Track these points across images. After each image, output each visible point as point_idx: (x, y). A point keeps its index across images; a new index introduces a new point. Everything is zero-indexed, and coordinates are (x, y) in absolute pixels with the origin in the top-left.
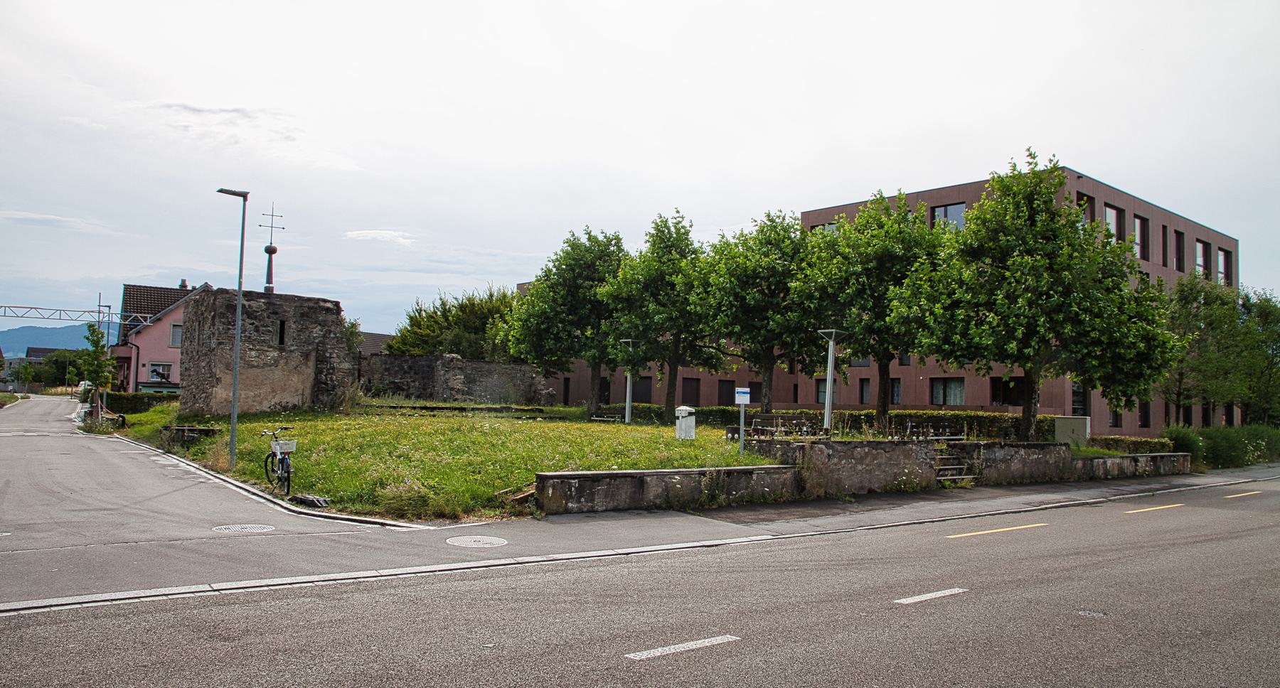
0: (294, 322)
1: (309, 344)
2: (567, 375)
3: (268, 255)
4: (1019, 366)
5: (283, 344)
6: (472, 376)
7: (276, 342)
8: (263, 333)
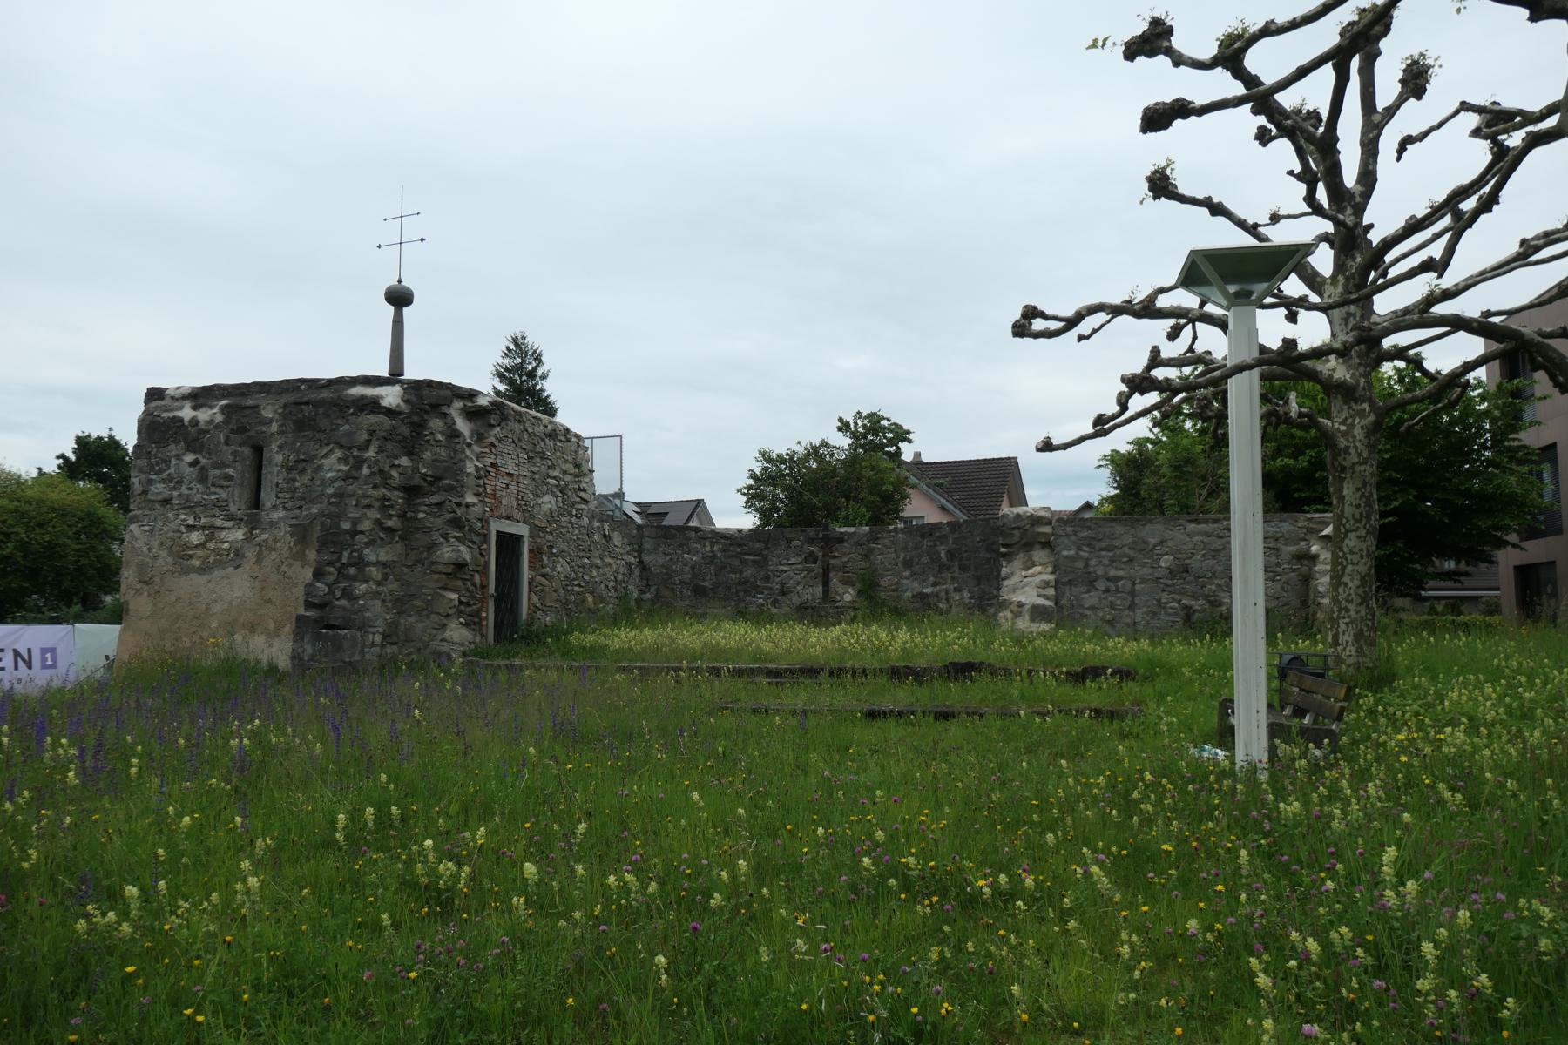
1: (312, 501)
2: (1536, 551)
4: (1476, 133)
5: (258, 509)
6: (1080, 564)
8: (214, 485)
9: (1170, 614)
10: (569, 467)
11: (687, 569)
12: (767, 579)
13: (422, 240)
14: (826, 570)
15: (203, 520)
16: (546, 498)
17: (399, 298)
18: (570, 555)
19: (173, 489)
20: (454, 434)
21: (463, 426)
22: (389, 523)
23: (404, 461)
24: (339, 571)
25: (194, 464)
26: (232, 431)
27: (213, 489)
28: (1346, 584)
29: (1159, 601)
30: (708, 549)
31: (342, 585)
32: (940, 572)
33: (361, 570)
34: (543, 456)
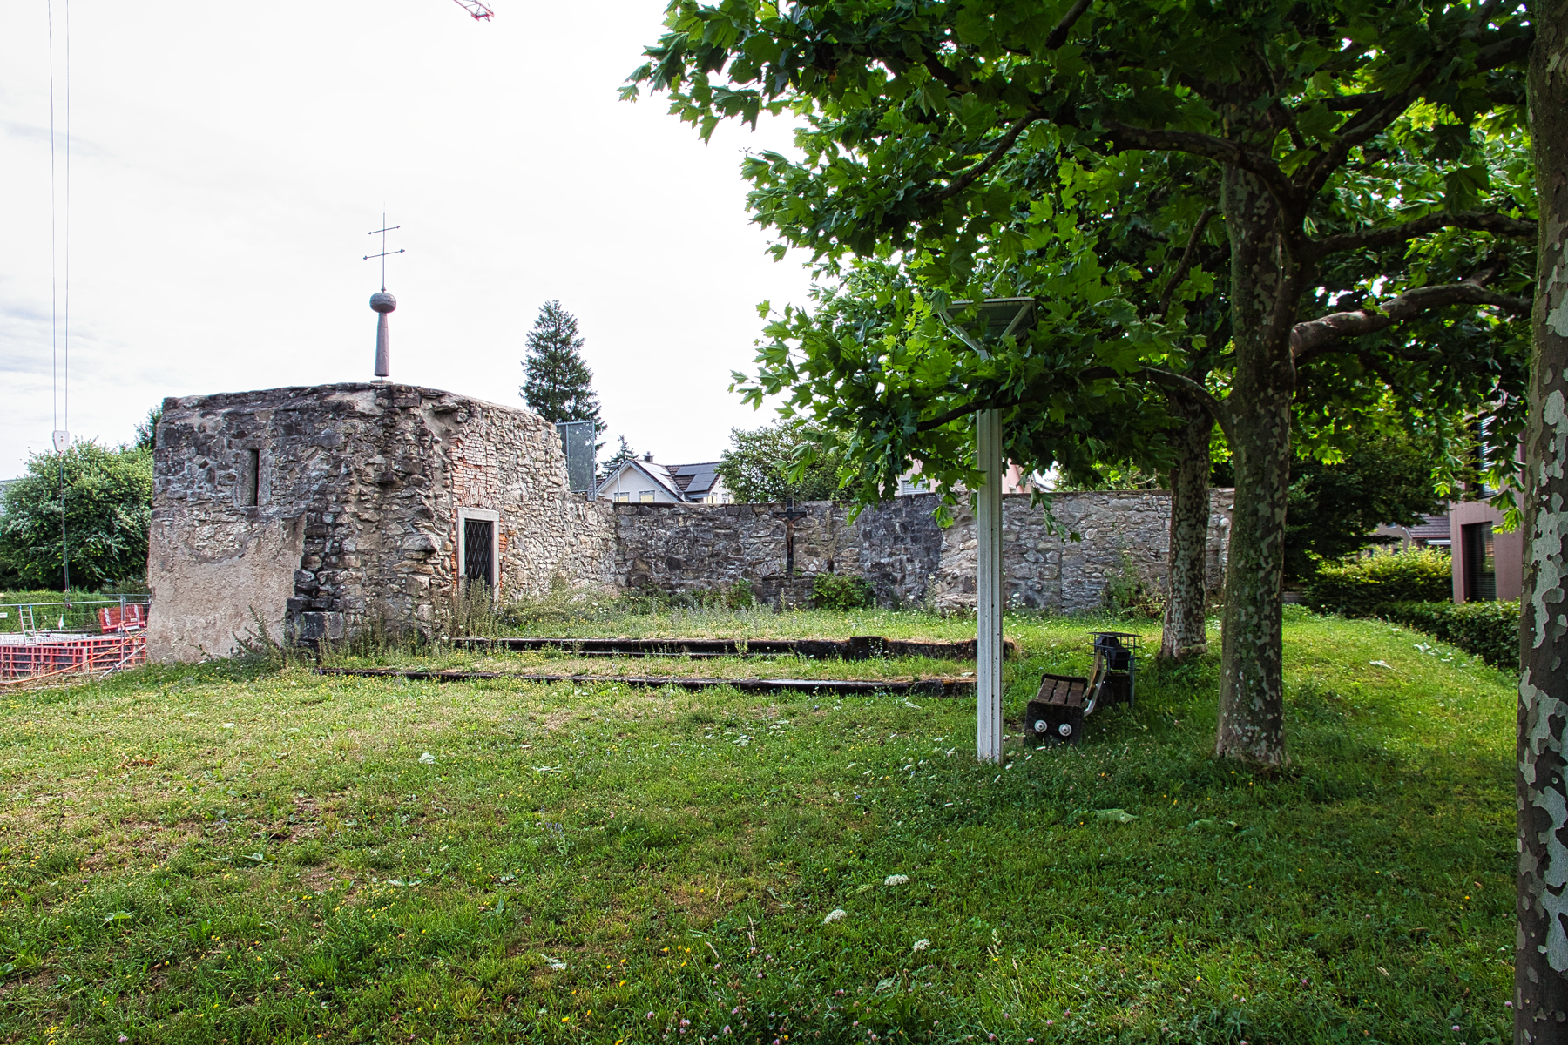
0: (273, 450)
3: (377, 314)
7: (240, 503)
8: (220, 484)
9: (1094, 583)
10: (541, 455)
11: (661, 544)
12: (738, 550)
13: (402, 251)
14: (791, 543)
15: (212, 515)
16: (516, 485)
17: (383, 306)
18: (542, 535)
19: (188, 487)
20: (422, 433)
21: (434, 427)
22: (366, 516)
23: (379, 459)
24: (323, 559)
25: (203, 466)
26: (234, 436)
27: (219, 488)
28: (1178, 568)
29: (1084, 572)
30: (681, 524)
31: (325, 572)
32: (895, 543)
33: (341, 559)
34: (511, 446)
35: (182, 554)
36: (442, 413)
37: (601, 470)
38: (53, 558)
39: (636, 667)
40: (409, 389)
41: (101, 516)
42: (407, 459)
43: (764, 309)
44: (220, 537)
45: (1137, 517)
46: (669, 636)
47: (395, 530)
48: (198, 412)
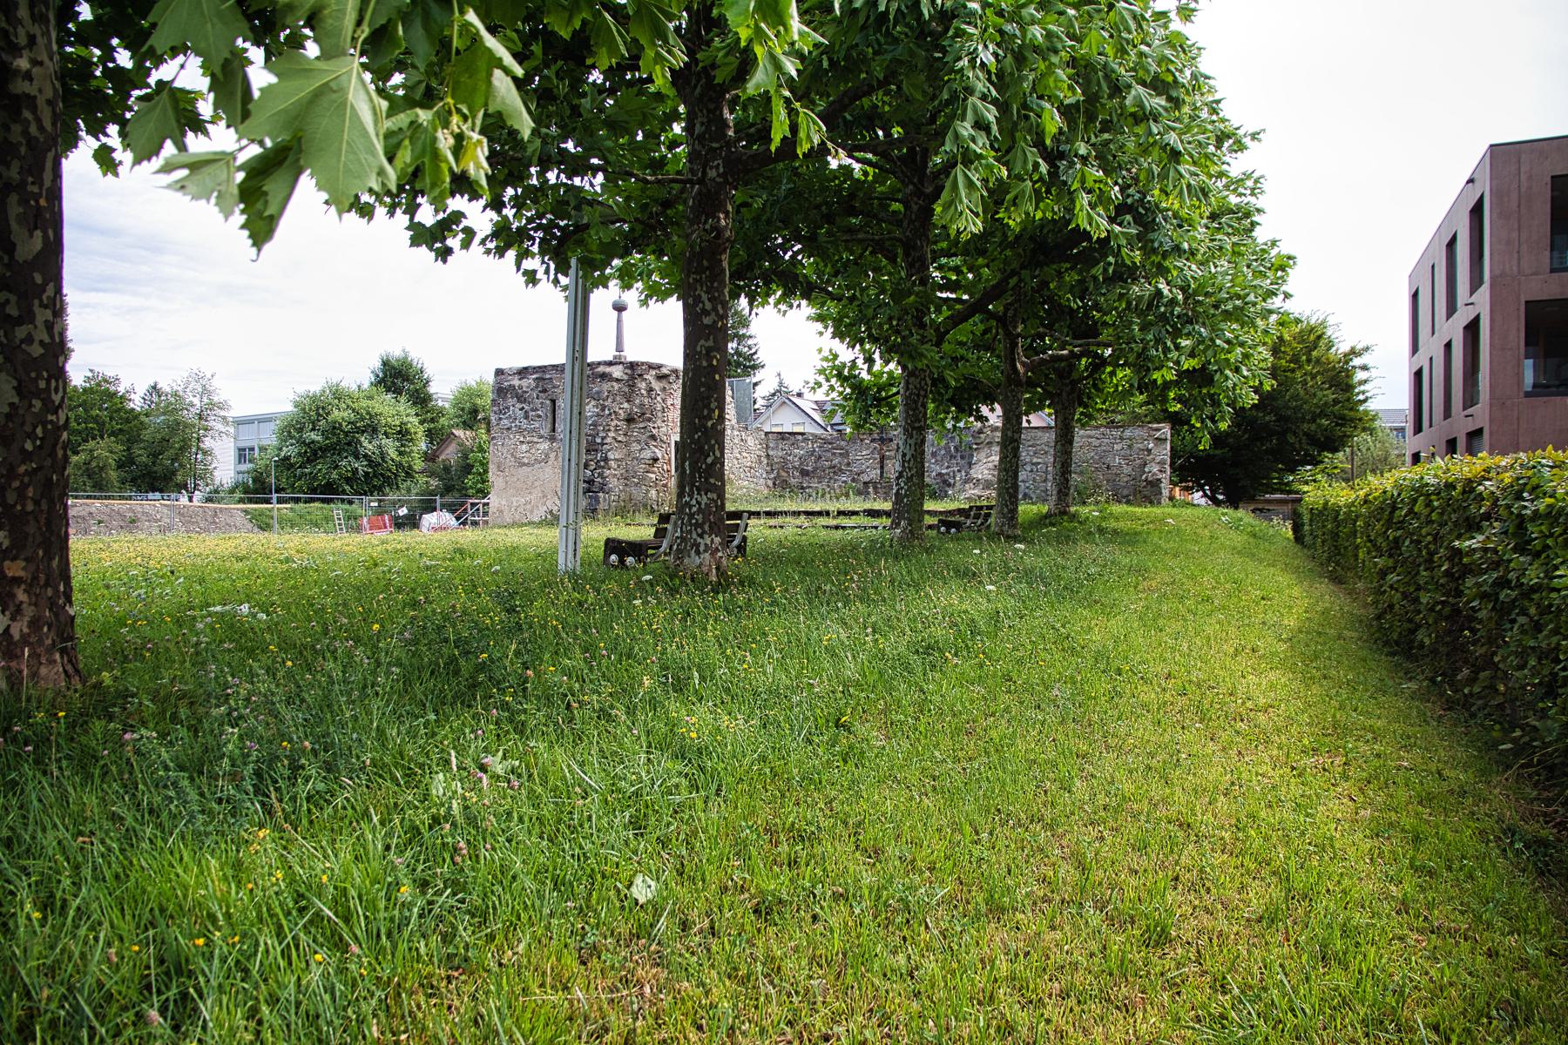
7: (545, 431)
12: (848, 464)
21: (656, 385)
23: (626, 405)
35: (510, 461)
36: (660, 378)
37: (760, 402)
38: (315, 478)
39: (772, 522)
40: (643, 364)
41: (349, 444)
42: (642, 405)
43: (820, 351)
44: (533, 451)
45: (1096, 443)
46: (794, 508)
47: (635, 447)
48: (517, 377)
